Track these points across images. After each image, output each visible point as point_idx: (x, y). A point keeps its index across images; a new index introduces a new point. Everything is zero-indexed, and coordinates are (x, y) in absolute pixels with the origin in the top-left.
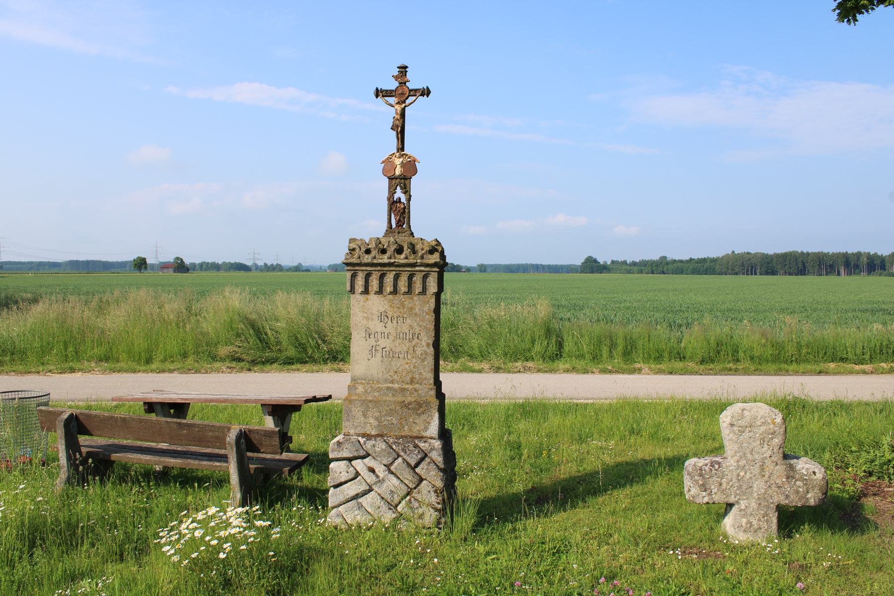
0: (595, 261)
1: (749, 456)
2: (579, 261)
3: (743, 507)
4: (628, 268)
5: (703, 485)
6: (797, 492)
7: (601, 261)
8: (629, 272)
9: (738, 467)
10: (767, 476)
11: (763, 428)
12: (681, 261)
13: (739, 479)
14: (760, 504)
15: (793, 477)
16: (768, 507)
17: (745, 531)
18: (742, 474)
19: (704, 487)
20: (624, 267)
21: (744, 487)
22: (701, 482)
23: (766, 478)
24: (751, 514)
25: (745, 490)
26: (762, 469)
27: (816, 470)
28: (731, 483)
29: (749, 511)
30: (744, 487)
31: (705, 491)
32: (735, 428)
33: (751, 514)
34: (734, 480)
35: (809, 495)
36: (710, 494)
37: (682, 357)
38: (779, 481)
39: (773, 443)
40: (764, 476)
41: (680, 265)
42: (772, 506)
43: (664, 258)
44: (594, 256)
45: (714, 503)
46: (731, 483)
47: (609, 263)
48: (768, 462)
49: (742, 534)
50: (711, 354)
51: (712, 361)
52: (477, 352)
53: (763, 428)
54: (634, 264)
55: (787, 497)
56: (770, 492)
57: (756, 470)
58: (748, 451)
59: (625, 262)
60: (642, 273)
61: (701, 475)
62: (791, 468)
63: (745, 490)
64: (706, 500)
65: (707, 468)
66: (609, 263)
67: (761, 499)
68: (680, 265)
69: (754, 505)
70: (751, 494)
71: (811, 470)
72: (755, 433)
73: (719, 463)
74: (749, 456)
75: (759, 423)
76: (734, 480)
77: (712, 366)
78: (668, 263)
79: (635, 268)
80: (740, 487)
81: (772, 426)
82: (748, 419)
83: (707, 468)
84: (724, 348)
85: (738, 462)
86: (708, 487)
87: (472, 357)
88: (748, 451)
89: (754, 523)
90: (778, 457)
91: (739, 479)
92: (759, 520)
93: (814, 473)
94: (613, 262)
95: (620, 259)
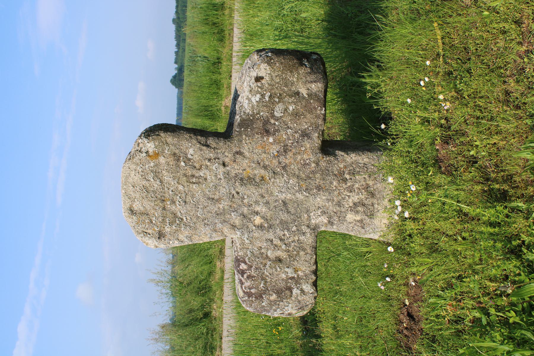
0: (174, 77)
1: (224, 204)
2: (174, 91)
3: (324, 219)
4: (181, 51)
5: (279, 292)
6: (296, 115)
7: (174, 72)
8: (184, 50)
9: (244, 228)
10: (263, 172)
11: (167, 177)
12: (177, 7)
13: (268, 226)
14: (319, 188)
15: (266, 122)
16: (325, 173)
17: (371, 216)
18: (258, 220)
19: (284, 292)
20: (180, 54)
21: (284, 216)
22: (274, 297)
23: (267, 175)
24: (339, 204)
25: (290, 215)
26: (250, 180)
27: (254, 74)
28: (277, 242)
29: (331, 208)
30: (284, 216)
31: (290, 289)
32: (167, 229)
33: (339, 204)
34: (270, 236)
35: (304, 92)
36: (297, 281)
37: (218, 62)
38: (274, 149)
39: (196, 157)
40: (263, 178)
41: (179, 8)
42: (323, 164)
43: (174, 20)
44: (171, 78)
45: (315, 272)
46: (277, 242)
47: (176, 66)
48: (234, 169)
49: (376, 222)
50: (216, 31)
51: (222, 31)
52: (206, 267)
53: (167, 177)
54: (178, 45)
55: (305, 135)
56: (294, 167)
57: (250, 193)
58: (214, 208)
59: (177, 53)
60: (185, 40)
61: (259, 296)
62: (248, 123)
63: (290, 215)
64: (308, 288)
65: (248, 284)
66: (176, 66)
67: (308, 183)
68: (179, 8)
69: (320, 200)
70: (299, 204)
71: (254, 85)
72: (175, 192)
73: (238, 261)
74: (224, 204)
75: (156, 185)
76: (270, 236)
77: (227, 32)
78: (178, 18)
79: (181, 45)
80: (285, 225)
81: (162, 160)
82: (148, 205)
83: (248, 284)
84: (211, 19)
85: (234, 227)
86: (282, 285)
87: (210, 274)
88: (214, 208)
89: (355, 198)
90: (225, 150)
91: (268, 226)
92: (351, 190)
93: (258, 79)
94: (176, 62)
95: (173, 57)
